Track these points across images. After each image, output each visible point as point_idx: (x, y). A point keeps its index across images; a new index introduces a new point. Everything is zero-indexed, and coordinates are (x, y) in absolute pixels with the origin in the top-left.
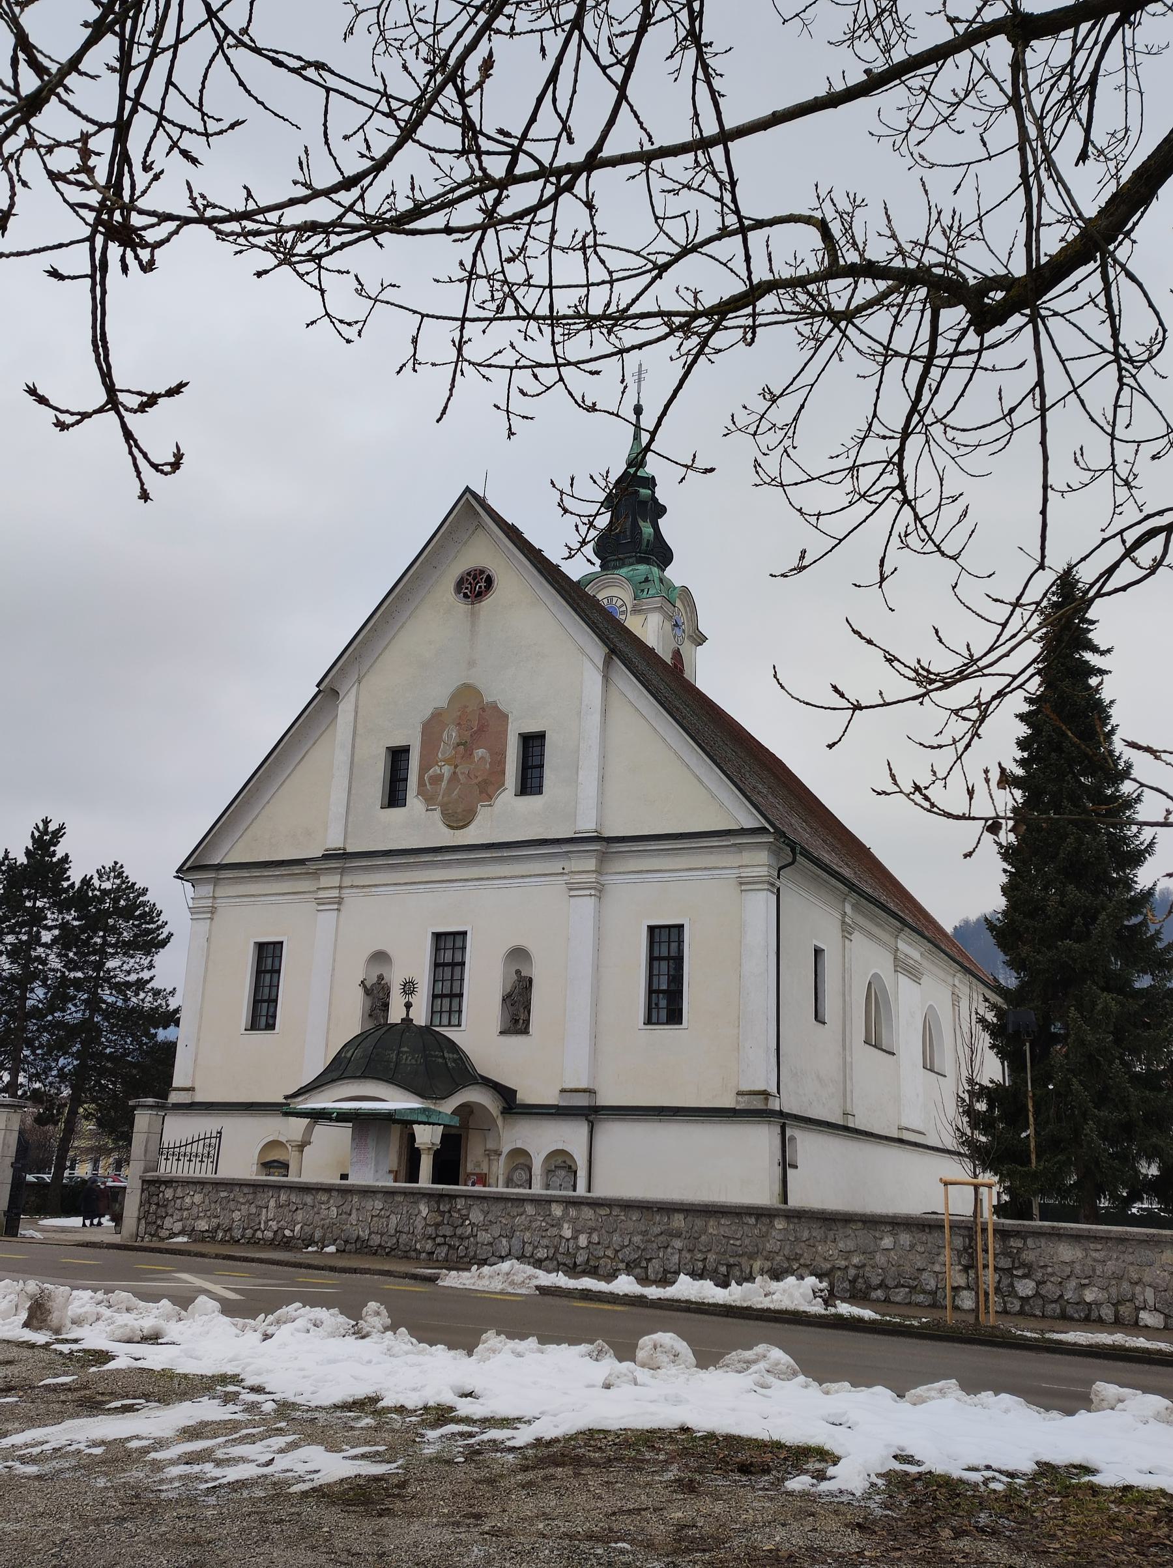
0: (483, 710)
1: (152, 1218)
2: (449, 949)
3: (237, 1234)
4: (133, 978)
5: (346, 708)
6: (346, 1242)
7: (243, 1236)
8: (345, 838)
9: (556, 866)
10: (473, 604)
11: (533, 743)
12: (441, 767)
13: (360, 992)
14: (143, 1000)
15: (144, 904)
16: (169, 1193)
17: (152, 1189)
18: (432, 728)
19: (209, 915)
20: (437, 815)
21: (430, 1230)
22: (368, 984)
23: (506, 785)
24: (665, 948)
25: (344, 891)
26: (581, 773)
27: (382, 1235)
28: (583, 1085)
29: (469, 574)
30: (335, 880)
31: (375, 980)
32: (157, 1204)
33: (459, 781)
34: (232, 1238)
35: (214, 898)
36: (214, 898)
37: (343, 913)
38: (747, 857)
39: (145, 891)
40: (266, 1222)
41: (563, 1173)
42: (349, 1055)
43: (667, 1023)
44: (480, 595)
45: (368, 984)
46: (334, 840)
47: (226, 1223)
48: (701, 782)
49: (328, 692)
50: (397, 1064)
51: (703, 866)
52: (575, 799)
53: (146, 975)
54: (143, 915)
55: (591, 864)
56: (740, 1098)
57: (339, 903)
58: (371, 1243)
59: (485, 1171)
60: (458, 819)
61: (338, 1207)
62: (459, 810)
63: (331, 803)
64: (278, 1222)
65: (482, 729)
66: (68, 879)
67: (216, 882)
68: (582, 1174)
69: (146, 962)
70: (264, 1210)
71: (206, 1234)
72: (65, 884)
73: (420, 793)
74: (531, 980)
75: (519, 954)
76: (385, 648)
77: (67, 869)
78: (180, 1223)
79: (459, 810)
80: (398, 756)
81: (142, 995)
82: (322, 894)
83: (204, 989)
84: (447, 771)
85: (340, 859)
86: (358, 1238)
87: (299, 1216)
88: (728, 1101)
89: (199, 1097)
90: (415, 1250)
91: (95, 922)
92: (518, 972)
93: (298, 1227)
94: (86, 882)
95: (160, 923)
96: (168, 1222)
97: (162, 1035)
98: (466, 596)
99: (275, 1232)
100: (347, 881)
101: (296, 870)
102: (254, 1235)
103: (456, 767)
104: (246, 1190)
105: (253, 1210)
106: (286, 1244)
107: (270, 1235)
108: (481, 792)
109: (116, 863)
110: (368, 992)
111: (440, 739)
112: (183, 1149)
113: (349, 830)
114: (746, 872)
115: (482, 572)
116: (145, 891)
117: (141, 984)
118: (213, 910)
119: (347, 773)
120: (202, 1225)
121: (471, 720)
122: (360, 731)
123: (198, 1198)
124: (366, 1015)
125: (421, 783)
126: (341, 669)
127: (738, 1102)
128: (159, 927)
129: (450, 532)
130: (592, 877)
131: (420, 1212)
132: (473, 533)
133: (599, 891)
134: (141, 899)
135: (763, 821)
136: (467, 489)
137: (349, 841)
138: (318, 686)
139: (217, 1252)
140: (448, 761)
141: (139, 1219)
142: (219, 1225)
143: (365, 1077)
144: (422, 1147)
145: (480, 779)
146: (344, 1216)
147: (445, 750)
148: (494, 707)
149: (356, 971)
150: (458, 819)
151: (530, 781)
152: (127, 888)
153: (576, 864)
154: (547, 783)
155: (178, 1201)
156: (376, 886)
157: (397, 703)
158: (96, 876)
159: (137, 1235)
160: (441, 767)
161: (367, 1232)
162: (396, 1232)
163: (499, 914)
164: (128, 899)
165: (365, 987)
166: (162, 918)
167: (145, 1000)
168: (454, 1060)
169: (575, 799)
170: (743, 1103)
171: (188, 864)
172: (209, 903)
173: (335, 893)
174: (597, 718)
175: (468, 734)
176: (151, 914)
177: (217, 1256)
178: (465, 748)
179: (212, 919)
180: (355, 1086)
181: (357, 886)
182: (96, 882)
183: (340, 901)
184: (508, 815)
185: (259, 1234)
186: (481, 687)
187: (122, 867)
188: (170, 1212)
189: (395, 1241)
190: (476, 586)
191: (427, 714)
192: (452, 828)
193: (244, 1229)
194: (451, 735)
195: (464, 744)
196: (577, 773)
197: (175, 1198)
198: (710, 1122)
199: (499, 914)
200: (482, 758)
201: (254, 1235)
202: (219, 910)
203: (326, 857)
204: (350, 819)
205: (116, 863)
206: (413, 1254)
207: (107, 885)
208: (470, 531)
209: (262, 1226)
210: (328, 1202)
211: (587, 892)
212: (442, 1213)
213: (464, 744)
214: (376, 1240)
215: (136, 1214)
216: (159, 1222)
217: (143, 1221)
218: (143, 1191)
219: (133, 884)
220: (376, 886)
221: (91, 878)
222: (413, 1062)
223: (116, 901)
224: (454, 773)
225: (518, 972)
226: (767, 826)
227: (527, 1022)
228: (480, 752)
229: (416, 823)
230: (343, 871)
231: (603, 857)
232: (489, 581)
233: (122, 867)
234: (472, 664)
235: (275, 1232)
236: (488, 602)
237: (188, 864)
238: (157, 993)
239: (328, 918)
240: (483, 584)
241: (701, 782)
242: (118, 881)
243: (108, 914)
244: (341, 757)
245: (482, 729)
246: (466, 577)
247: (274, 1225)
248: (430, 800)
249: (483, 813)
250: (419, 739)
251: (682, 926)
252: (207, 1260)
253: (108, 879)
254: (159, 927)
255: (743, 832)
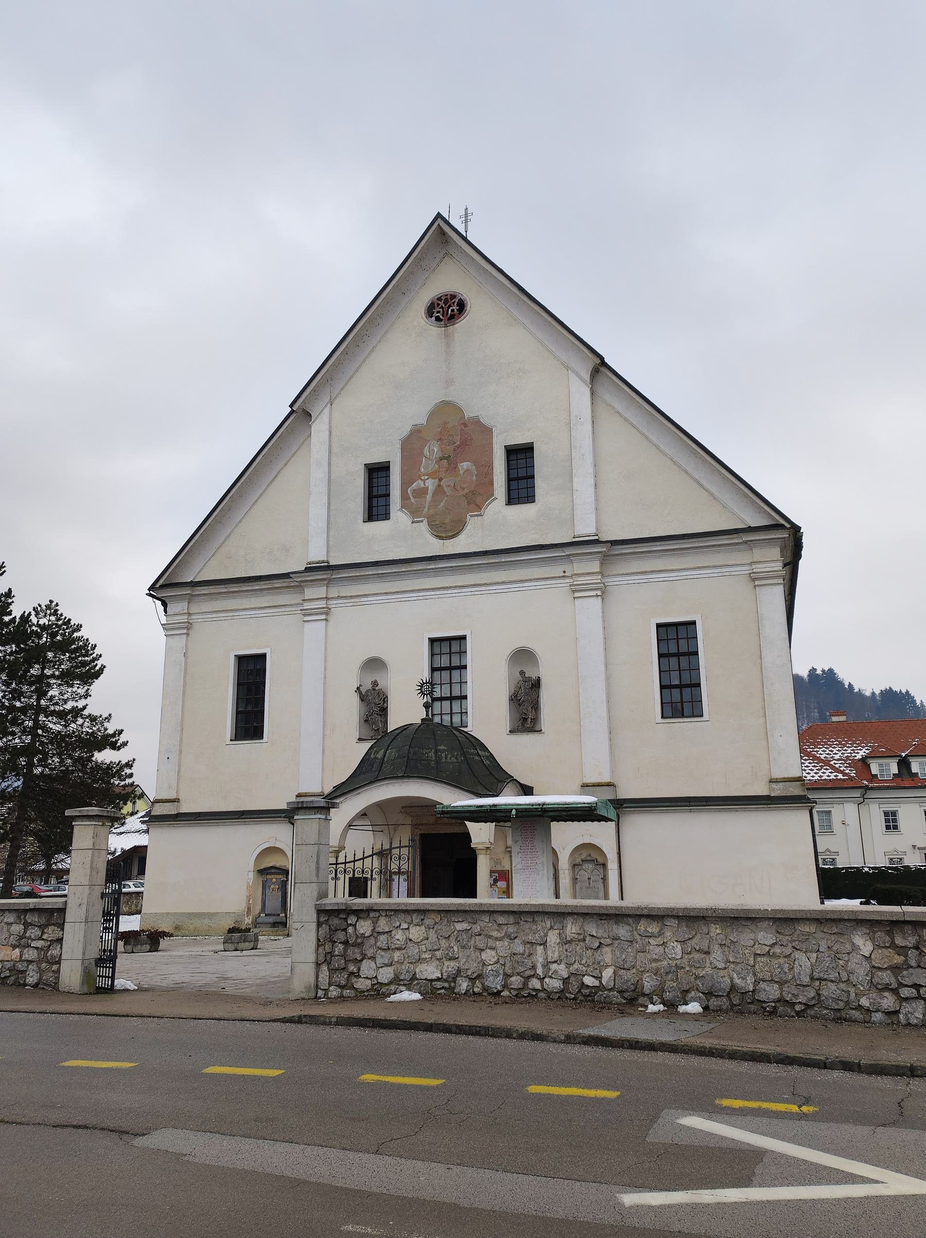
0: (465, 425)
1: (338, 963)
2: (448, 652)
3: (495, 983)
4: (68, 706)
5: (319, 428)
6: (709, 994)
7: (505, 986)
8: (328, 552)
9: (557, 570)
10: (446, 326)
11: (521, 457)
12: (424, 481)
13: (356, 698)
14: (82, 726)
15: (79, 639)
16: (364, 927)
17: (335, 921)
18: (412, 444)
19: (185, 631)
20: (424, 526)
21: (886, 977)
22: (363, 690)
23: (496, 493)
24: (677, 644)
25: (331, 602)
26: (575, 480)
27: (781, 983)
28: (606, 779)
29: (439, 299)
30: (321, 591)
31: (370, 687)
32: (346, 943)
33: (444, 493)
34: (485, 989)
35: (189, 614)
36: (189, 614)
37: (331, 623)
38: (758, 554)
39: (79, 628)
40: (546, 965)
41: (590, 866)
42: (380, 755)
43: (672, 717)
44: (452, 318)
45: (363, 690)
46: (317, 554)
47: (473, 968)
48: (702, 486)
49: (300, 414)
50: (438, 762)
51: (711, 564)
52: (572, 501)
53: (80, 704)
54: (79, 649)
55: (595, 566)
56: (774, 785)
57: (327, 614)
58: (762, 996)
59: (507, 867)
60: (445, 528)
61: (683, 942)
62: (447, 521)
63: (311, 517)
64: (569, 965)
65: (465, 443)
66: (10, 613)
67: (190, 598)
68: (612, 866)
69: (81, 691)
70: (540, 949)
71: (438, 985)
72: (7, 619)
73: (405, 504)
74: (538, 681)
75: (523, 656)
76: (356, 371)
77: (10, 604)
78: (390, 970)
79: (447, 521)
80: (377, 474)
81: (80, 721)
82: (307, 606)
83: (183, 702)
84: (431, 484)
85: (323, 571)
86: (733, 988)
87: (607, 955)
88: (760, 789)
89: (184, 809)
90: (859, 1007)
91: (37, 655)
92: (522, 673)
93: (608, 974)
94: (25, 619)
95: (94, 655)
96: (367, 968)
97: (105, 756)
98: (438, 319)
99: (566, 981)
100: (334, 592)
101: (278, 583)
102: (525, 984)
103: (440, 480)
104: (501, 920)
105: (521, 949)
106: (589, 1000)
107: (554, 984)
108: (469, 503)
109: (51, 602)
110: (363, 698)
111: (421, 454)
112: (359, 864)
113: (331, 543)
114: (758, 568)
115: (453, 296)
116: (79, 628)
117: (77, 712)
118: (189, 626)
119: (325, 489)
120: (430, 971)
121: (453, 436)
122: (335, 449)
123: (416, 933)
124: (363, 721)
125: (404, 496)
126: (314, 390)
127: (771, 789)
128: (94, 660)
129: (420, 259)
130: (597, 579)
131: (855, 948)
132: (441, 261)
133: (603, 592)
134: (75, 635)
135: (777, 517)
136: (439, 216)
137: (332, 554)
138: (291, 406)
139: (569, 1030)
140: (431, 475)
141: (318, 965)
142: (459, 971)
143: (408, 777)
144: (480, 847)
145: (466, 491)
146: (697, 956)
147: (427, 465)
148: (477, 422)
149: (349, 680)
150: (445, 528)
151: (521, 488)
152: (64, 624)
153: (579, 567)
154: (539, 491)
155: (382, 938)
156: (365, 596)
157: (375, 419)
158: (33, 613)
159: (317, 987)
160: (424, 481)
161: (750, 980)
162: (812, 979)
163: (496, 620)
164: (63, 635)
165: (360, 693)
166: (97, 651)
167: (80, 726)
168: (487, 758)
169: (572, 501)
170: (778, 790)
171: (161, 582)
172: (184, 618)
173: (322, 604)
174: (589, 427)
175: (451, 448)
176: (85, 648)
177: (570, 1039)
178: (449, 461)
179: (187, 634)
180: (397, 786)
181: (342, 597)
182: (34, 619)
183: (327, 612)
184: (500, 522)
185: (535, 983)
186: (461, 404)
187: (57, 605)
188: (370, 953)
189: (812, 993)
190: (447, 310)
191: (406, 431)
192: (441, 538)
193: (507, 976)
194: (433, 450)
195: (448, 458)
196: (571, 480)
197: (376, 934)
198: (745, 810)
199: (496, 620)
200: (467, 470)
201: (525, 984)
202: (195, 626)
203: (307, 570)
204: (331, 534)
205: (51, 602)
206: (856, 1014)
207: (43, 621)
208: (438, 260)
209: (540, 971)
210: (661, 934)
211: (594, 593)
212: (902, 950)
213: (448, 458)
214: (771, 992)
215: (312, 958)
216: (352, 968)
217: (325, 968)
218: (319, 924)
219: (69, 620)
220: (365, 596)
221: (30, 614)
222: (454, 759)
223: (53, 635)
224: (439, 486)
225: (522, 673)
226: (782, 522)
227: (536, 720)
228: (465, 465)
229: (402, 534)
230: (329, 582)
231: (605, 559)
232: (462, 306)
233: (57, 605)
234: (449, 382)
235: (566, 981)
236: (461, 325)
237: (161, 582)
238: (93, 719)
239: (315, 630)
240: (455, 308)
241: (702, 486)
242: (53, 618)
243: (44, 649)
244: (318, 475)
245: (465, 443)
246: (436, 302)
247: (562, 970)
248: (414, 512)
249: (472, 523)
250: (399, 455)
251: (694, 623)
252: (551, 1047)
253: (45, 616)
254: (94, 660)
255: (750, 530)
